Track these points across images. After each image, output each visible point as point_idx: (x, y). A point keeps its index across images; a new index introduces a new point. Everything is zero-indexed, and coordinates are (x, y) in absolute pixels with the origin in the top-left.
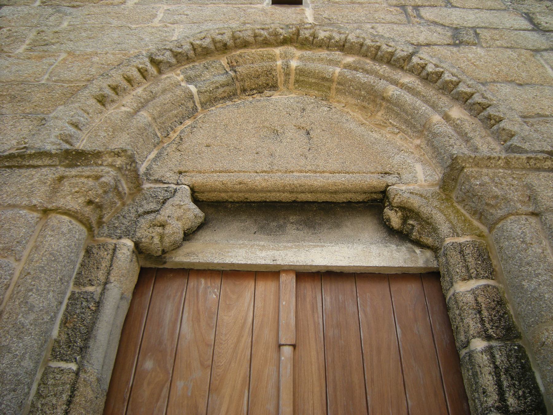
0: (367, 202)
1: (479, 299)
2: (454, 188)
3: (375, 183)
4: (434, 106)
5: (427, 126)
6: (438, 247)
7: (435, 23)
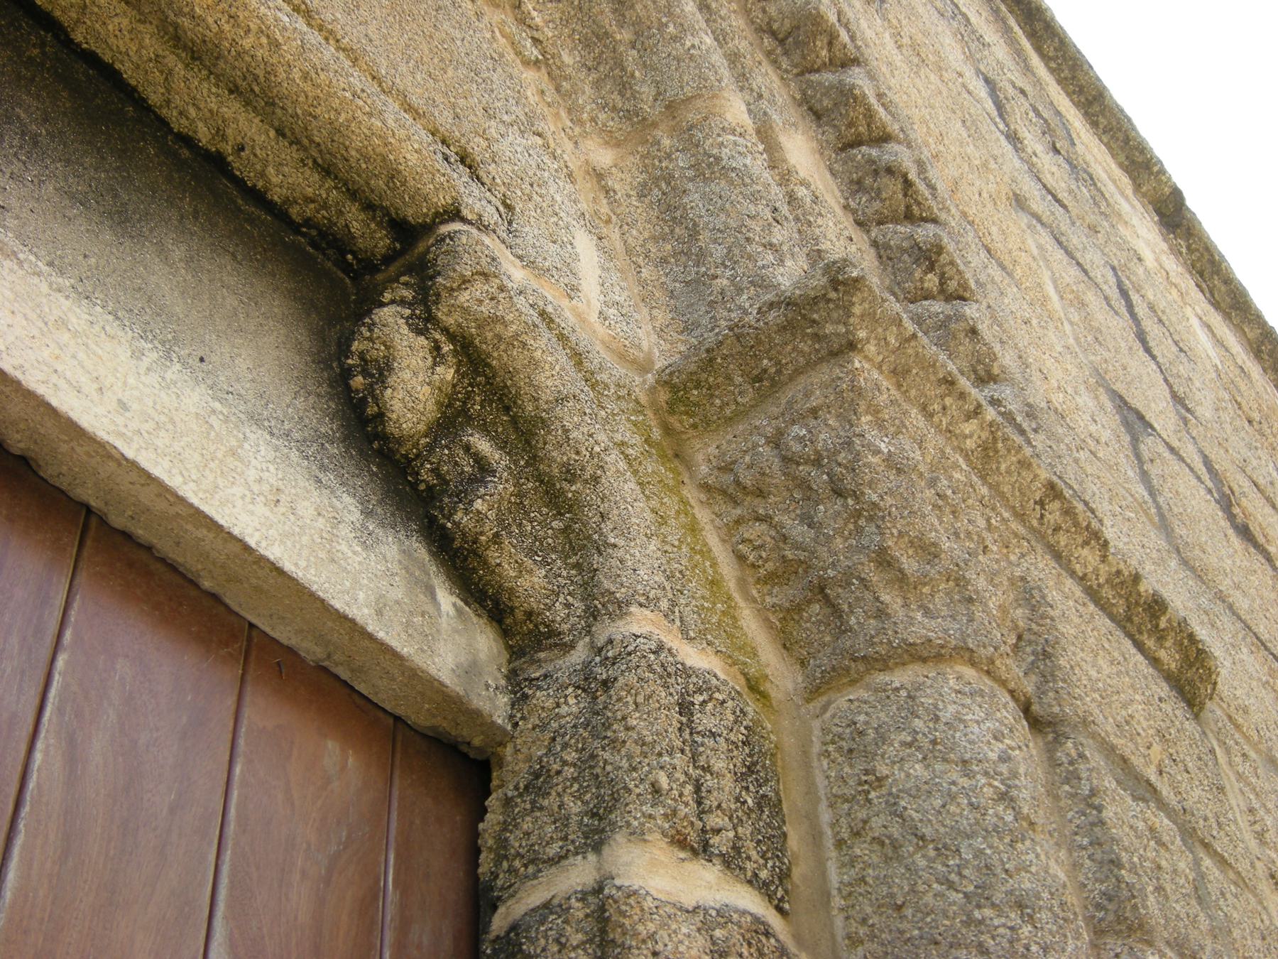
0: (294, 227)
2: (729, 421)
3: (413, 159)
5: (692, 117)
6: (553, 633)
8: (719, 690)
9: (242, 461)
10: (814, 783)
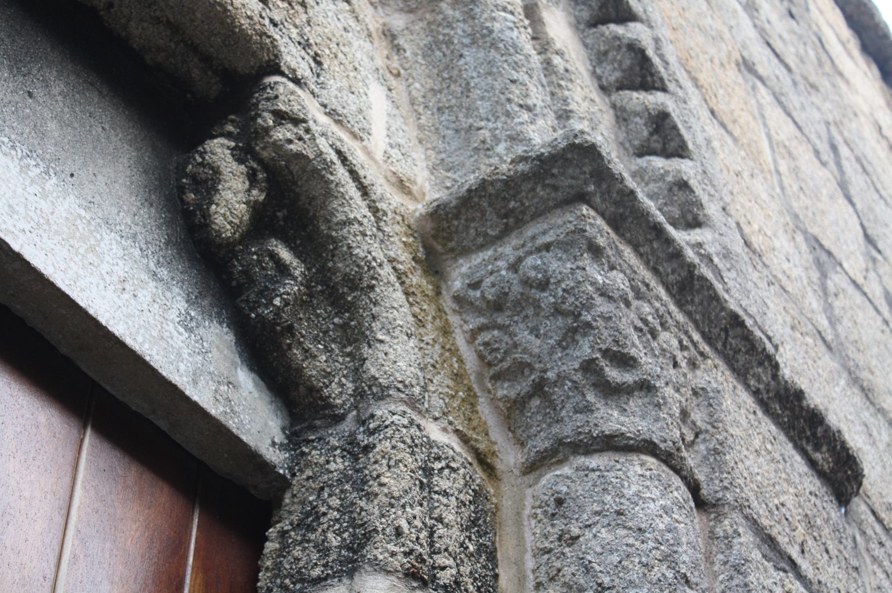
8: (454, 460)
9: (98, 256)
10: (523, 538)
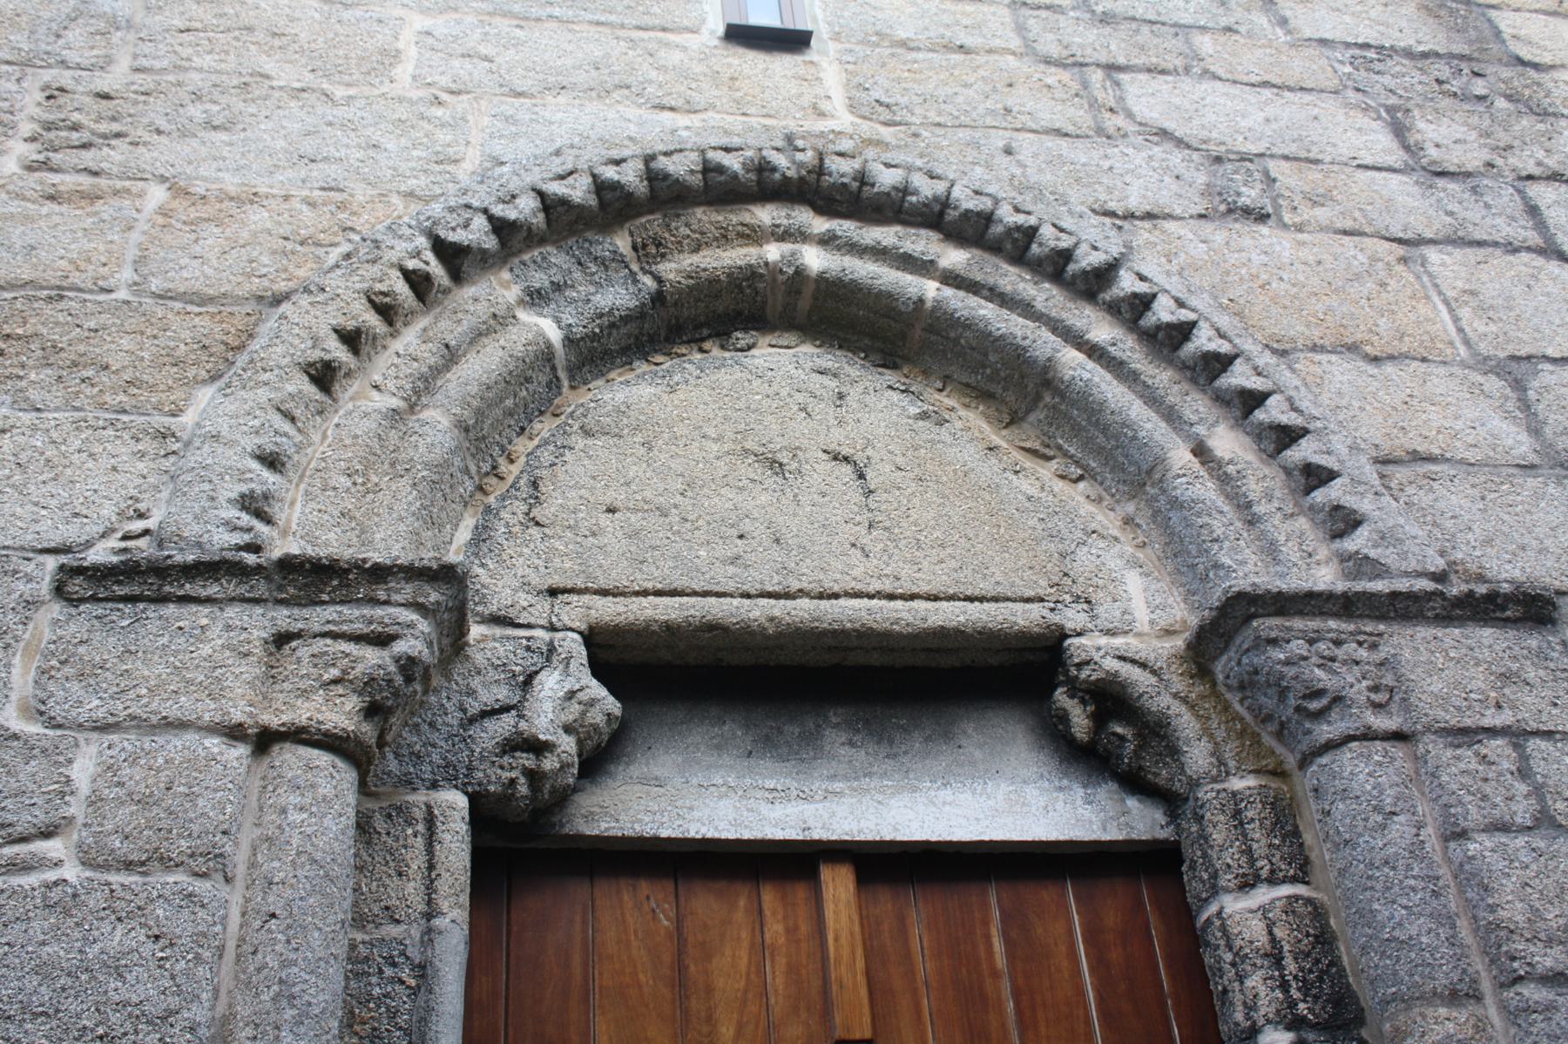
1: (1276, 931)
4: (1171, 416)
7: (1164, 134)
